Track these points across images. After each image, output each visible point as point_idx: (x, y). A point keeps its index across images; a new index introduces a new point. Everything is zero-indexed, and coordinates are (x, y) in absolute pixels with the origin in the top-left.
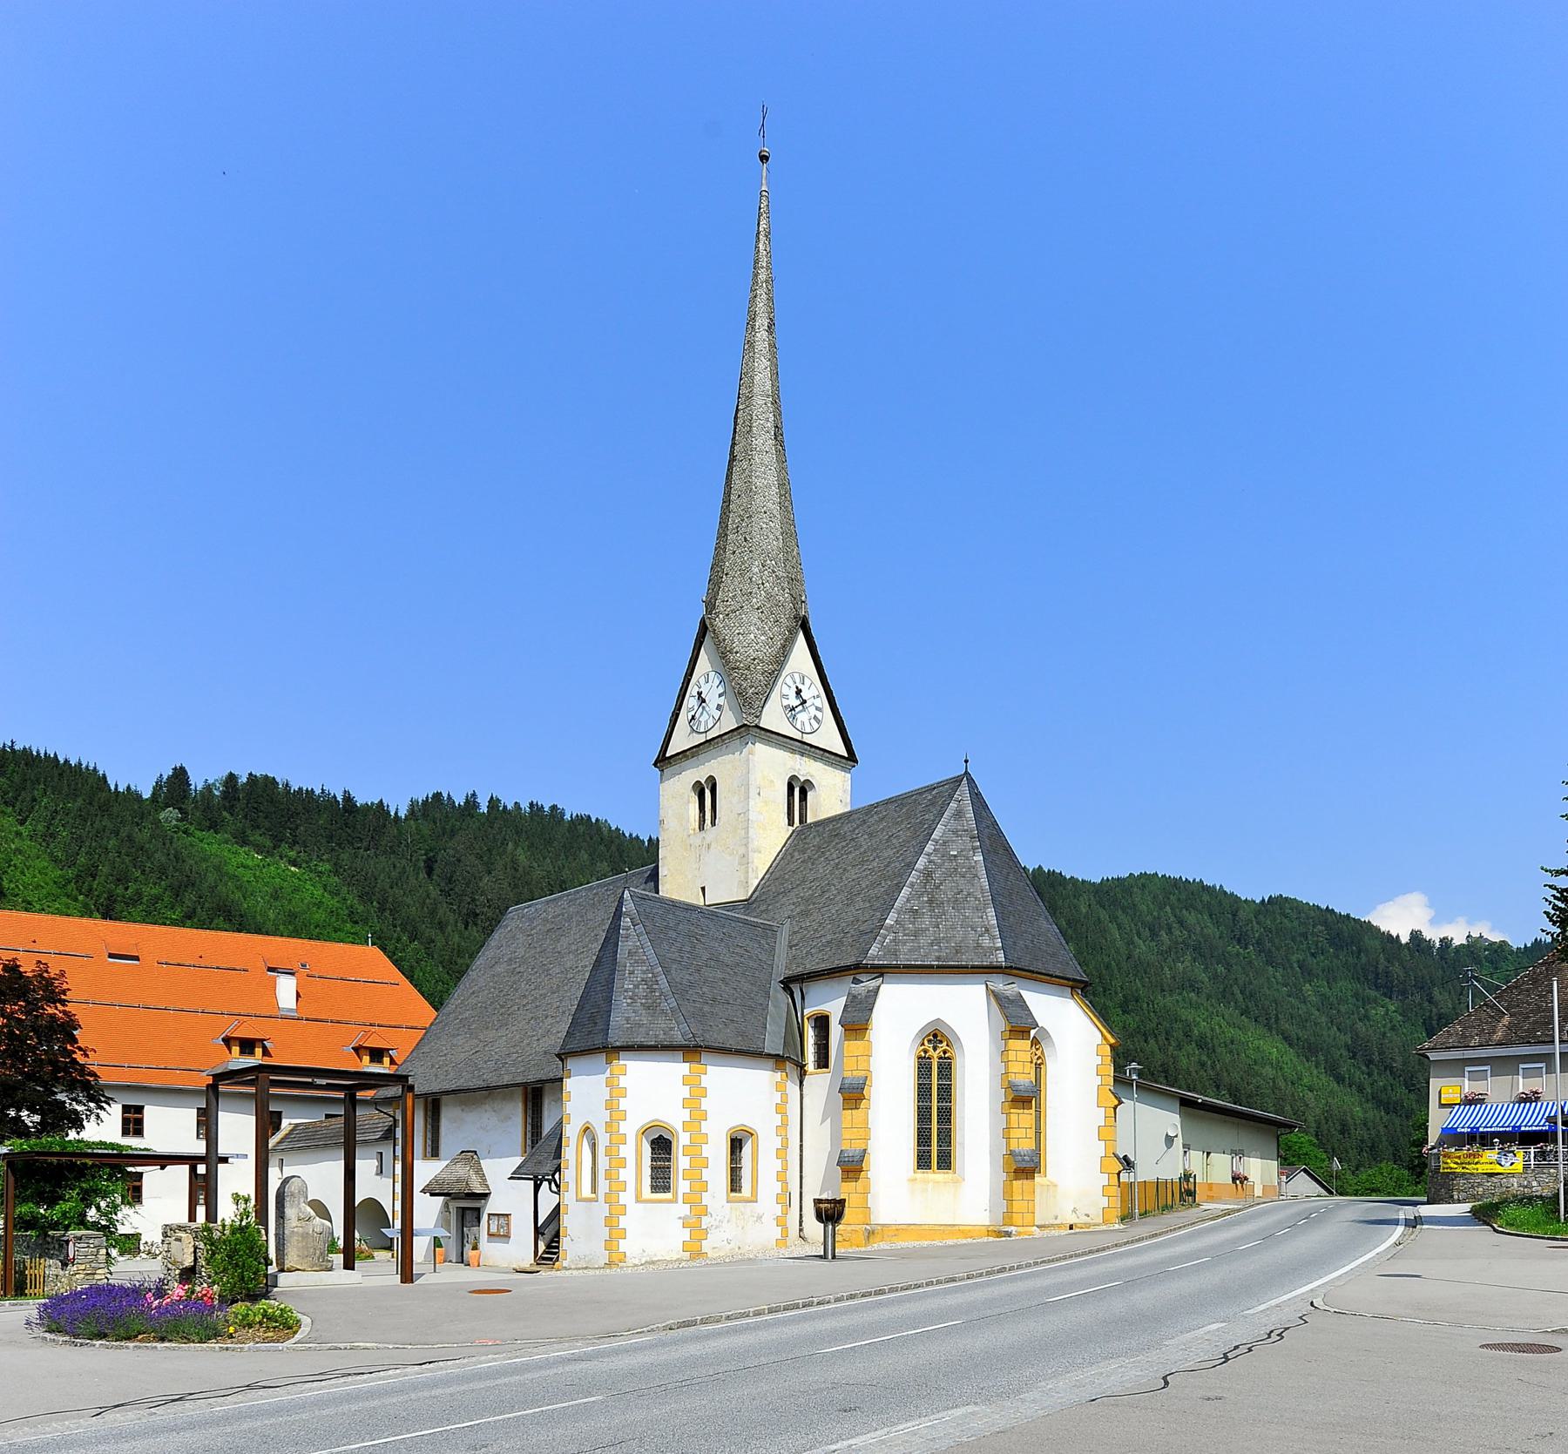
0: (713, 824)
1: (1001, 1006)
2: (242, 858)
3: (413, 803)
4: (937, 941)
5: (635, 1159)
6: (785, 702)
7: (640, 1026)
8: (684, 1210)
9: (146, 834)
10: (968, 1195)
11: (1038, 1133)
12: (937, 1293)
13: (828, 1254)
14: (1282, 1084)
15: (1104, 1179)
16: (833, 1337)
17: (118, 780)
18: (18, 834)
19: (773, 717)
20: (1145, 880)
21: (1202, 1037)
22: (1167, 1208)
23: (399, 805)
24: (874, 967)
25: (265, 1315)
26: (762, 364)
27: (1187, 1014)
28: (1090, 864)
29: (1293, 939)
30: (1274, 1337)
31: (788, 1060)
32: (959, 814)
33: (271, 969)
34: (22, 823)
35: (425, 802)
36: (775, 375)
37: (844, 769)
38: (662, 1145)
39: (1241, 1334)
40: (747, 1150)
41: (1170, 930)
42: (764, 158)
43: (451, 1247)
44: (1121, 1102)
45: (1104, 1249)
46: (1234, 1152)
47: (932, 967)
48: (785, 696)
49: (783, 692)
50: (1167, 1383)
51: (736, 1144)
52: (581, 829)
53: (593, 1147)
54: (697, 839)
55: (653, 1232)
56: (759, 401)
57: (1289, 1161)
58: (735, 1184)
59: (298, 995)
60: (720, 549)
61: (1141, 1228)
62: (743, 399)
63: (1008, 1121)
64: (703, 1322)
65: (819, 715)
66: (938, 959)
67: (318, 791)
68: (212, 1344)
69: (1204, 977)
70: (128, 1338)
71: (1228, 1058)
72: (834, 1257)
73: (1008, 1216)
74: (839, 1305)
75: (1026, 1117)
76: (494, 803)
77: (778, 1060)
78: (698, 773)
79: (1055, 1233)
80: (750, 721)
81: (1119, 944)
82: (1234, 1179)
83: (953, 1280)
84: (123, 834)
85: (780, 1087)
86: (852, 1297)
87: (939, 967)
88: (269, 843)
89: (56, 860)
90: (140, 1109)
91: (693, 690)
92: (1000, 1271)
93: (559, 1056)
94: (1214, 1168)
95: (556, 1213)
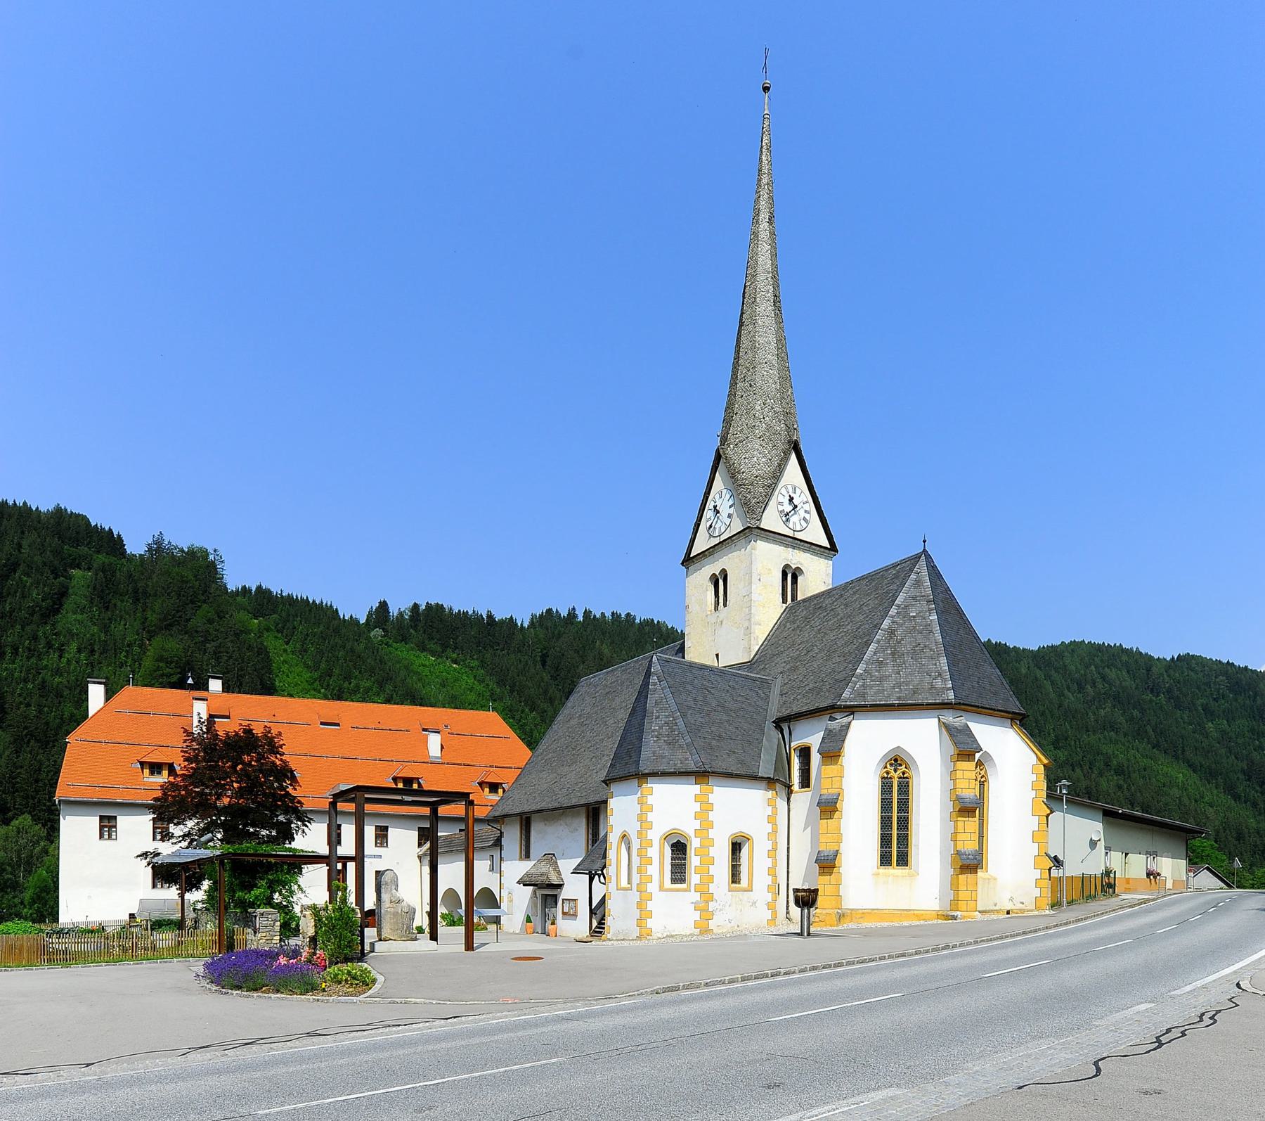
0: (725, 605)
1: (951, 736)
2: (422, 660)
3: (533, 617)
4: (899, 685)
5: (660, 857)
6: (781, 508)
7: (664, 757)
8: (696, 897)
9: (362, 646)
10: (923, 886)
11: (981, 837)
12: (887, 967)
13: (805, 932)
14: (1186, 801)
15: (1037, 874)
16: (787, 1005)
17: (345, 612)
18: (285, 651)
19: (771, 520)
20: (1074, 647)
21: (1120, 766)
22: (1091, 897)
23: (523, 619)
24: (846, 707)
25: (349, 973)
26: (764, 249)
27: (1106, 749)
28: (1028, 635)
29: (1198, 688)
30: (1207, 1021)
31: (778, 781)
32: (918, 584)
33: (424, 730)
34: (287, 643)
35: (541, 616)
36: (774, 256)
37: (827, 557)
38: (679, 848)
39: (1173, 1016)
40: (744, 852)
41: (1094, 684)
42: (766, 89)
43: (537, 920)
44: (1052, 812)
45: (1036, 931)
46: (1148, 853)
47: (893, 705)
48: (781, 504)
49: (779, 500)
50: (1099, 1070)
51: (736, 847)
52: (647, 629)
53: (629, 849)
54: (712, 619)
55: (672, 913)
56: (761, 277)
57: (1195, 861)
58: (735, 877)
59: (442, 747)
60: (732, 395)
61: (1067, 914)
62: (750, 277)
63: (956, 827)
64: (686, 988)
65: (807, 516)
66: (899, 698)
67: (471, 612)
68: (309, 997)
69: (1122, 719)
70: (256, 990)
71: (1141, 782)
72: (809, 934)
73: (955, 903)
74: (802, 975)
75: (971, 824)
76: (587, 614)
77: (770, 782)
78: (713, 568)
79: (995, 917)
80: (753, 523)
81: (1052, 696)
82: (1148, 875)
83: (903, 955)
84: (348, 647)
85: (770, 802)
86: (814, 968)
87: (899, 705)
88: (439, 649)
89: (307, 667)
90: (386, 828)
91: (710, 505)
92: (944, 948)
93: (604, 781)
94: (1131, 866)
95: (603, 901)
